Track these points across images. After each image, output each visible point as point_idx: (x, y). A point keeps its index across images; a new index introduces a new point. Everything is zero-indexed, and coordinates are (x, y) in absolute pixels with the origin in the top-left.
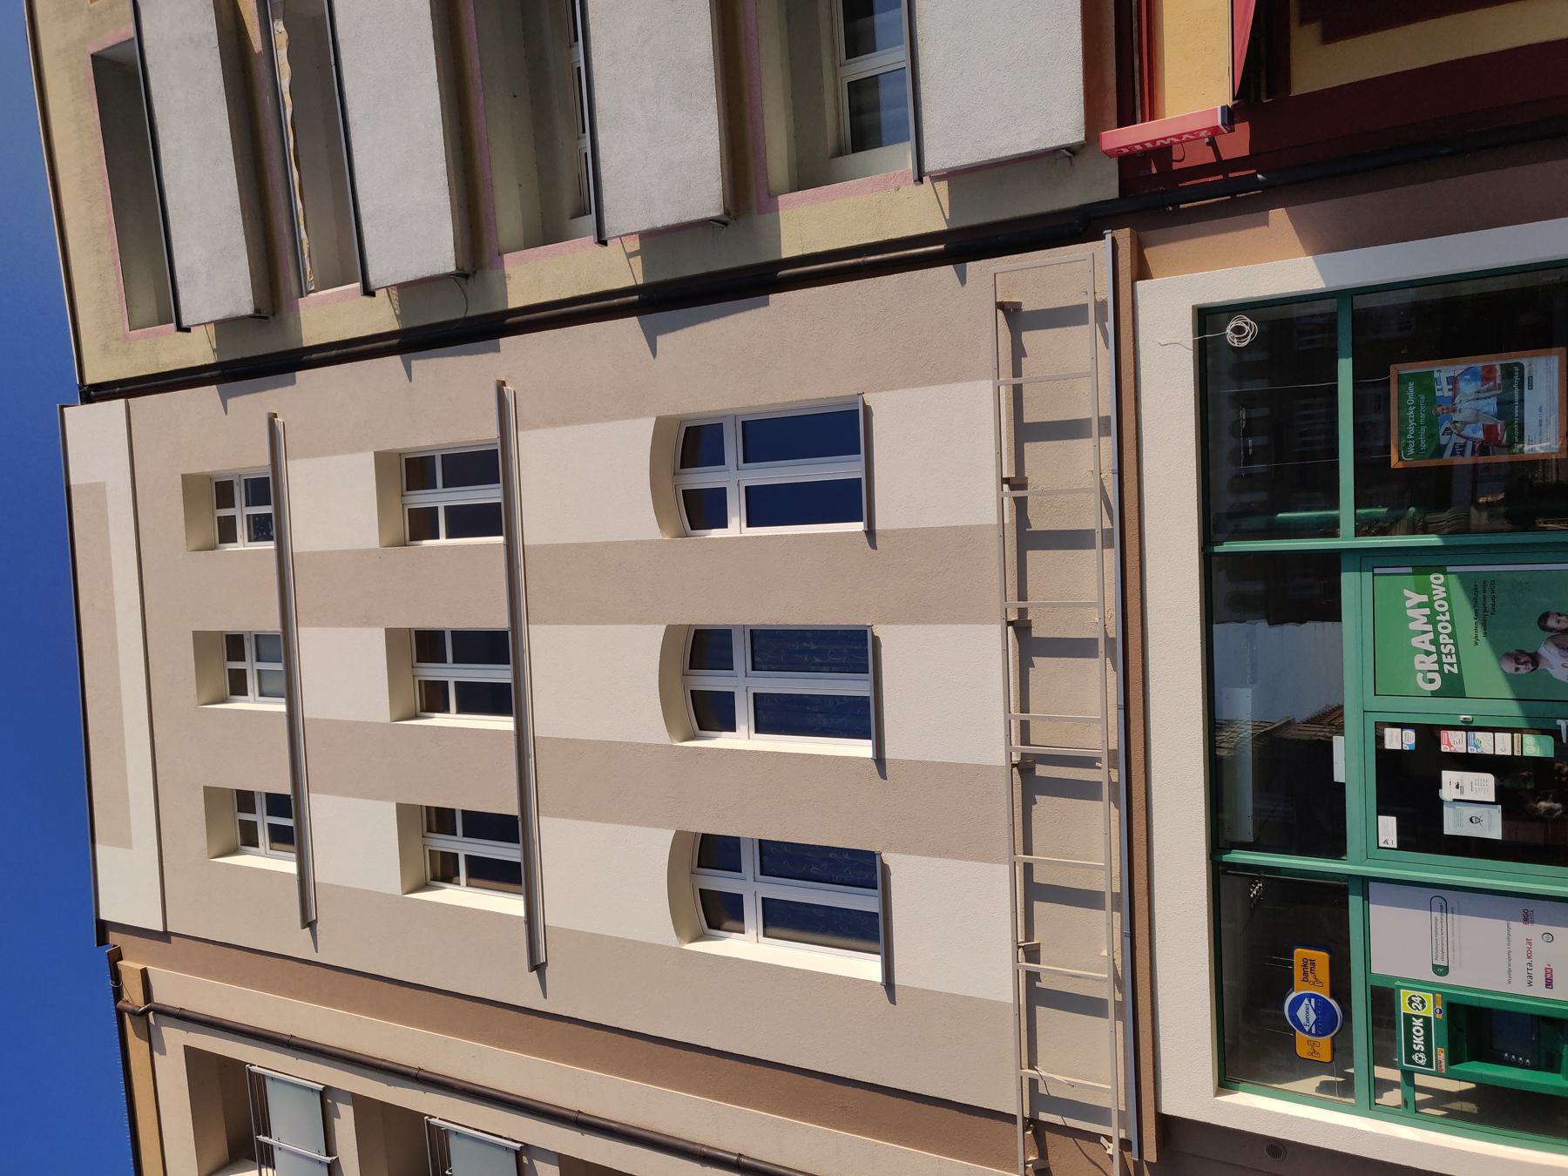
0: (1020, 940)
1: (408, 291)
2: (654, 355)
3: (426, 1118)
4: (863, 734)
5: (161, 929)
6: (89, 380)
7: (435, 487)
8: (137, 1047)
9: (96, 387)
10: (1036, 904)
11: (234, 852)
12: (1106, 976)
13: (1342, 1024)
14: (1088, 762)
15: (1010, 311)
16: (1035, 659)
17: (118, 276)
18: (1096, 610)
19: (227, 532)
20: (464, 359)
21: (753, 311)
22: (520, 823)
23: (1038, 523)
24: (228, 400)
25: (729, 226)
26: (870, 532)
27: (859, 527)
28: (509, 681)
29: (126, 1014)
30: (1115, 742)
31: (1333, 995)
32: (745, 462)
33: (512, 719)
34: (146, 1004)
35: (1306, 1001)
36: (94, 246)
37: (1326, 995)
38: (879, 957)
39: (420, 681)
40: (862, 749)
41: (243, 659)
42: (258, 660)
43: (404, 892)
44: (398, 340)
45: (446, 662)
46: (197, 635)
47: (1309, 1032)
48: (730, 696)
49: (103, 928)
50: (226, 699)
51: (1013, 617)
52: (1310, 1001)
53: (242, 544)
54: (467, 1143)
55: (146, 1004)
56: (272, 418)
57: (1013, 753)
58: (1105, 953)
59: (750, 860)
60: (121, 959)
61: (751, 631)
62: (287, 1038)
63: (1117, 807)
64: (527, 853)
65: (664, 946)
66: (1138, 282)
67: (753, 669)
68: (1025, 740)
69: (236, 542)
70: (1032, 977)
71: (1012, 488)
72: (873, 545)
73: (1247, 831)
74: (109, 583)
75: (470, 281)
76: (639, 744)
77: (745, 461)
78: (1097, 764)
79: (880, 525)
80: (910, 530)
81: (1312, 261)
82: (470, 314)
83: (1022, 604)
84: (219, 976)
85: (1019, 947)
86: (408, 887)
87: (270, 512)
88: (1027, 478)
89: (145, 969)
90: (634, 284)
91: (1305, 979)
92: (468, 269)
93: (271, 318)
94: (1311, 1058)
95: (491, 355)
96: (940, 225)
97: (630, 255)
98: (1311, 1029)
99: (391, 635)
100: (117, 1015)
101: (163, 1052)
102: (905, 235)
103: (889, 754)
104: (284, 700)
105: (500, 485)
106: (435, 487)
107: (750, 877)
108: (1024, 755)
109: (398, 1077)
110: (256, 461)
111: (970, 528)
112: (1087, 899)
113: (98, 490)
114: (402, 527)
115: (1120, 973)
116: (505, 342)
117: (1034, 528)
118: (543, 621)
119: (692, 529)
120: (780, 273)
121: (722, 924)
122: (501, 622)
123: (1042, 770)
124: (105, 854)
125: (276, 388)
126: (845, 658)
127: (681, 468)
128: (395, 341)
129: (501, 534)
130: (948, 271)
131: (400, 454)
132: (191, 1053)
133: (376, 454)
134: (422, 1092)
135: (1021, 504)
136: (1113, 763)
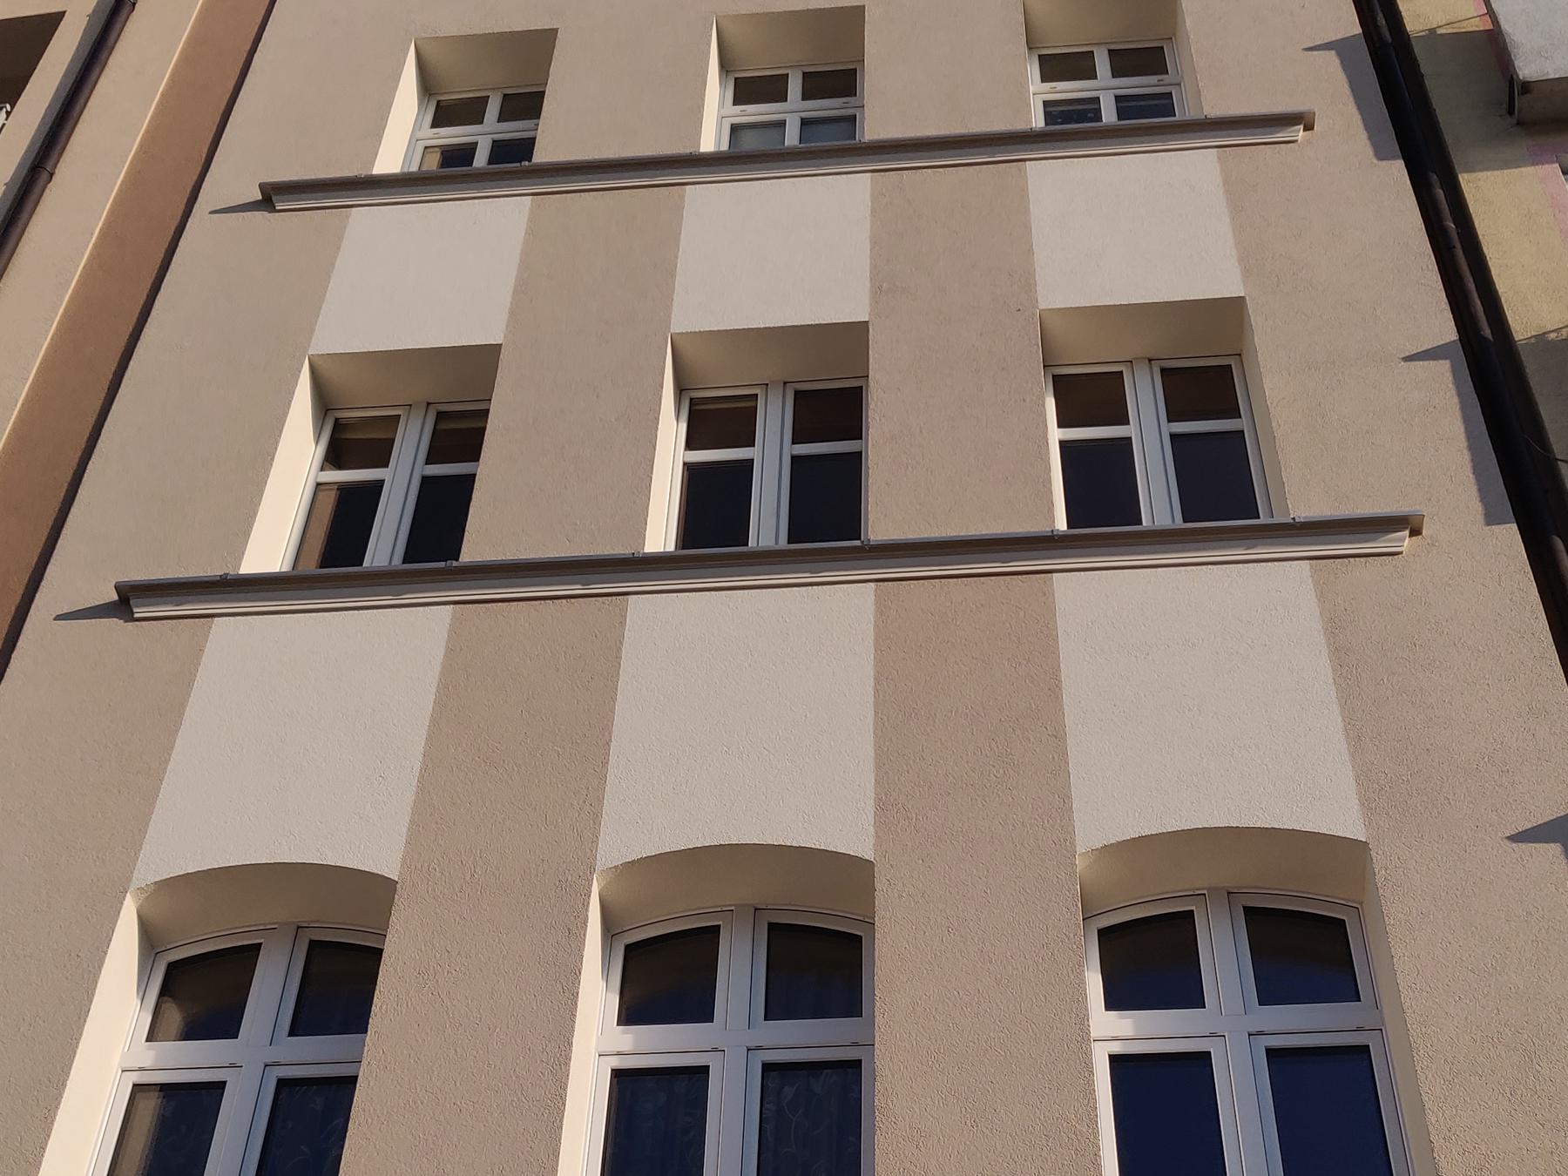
22: (442, 564)
24: (1333, 52)
28: (752, 542)
33: (671, 547)
42: (805, 123)
44: (1490, 337)
48: (703, 1013)
56: (1303, 120)
61: (857, 1064)
64: (384, 580)
69: (1042, 81)
77: (1271, 1053)
87: (1144, 524)
93: (1513, 120)
95: (1477, 507)
104: (724, 147)
105: (1179, 523)
107: (272, 1055)
114: (1085, 359)
122: (880, 525)
128: (1487, 332)
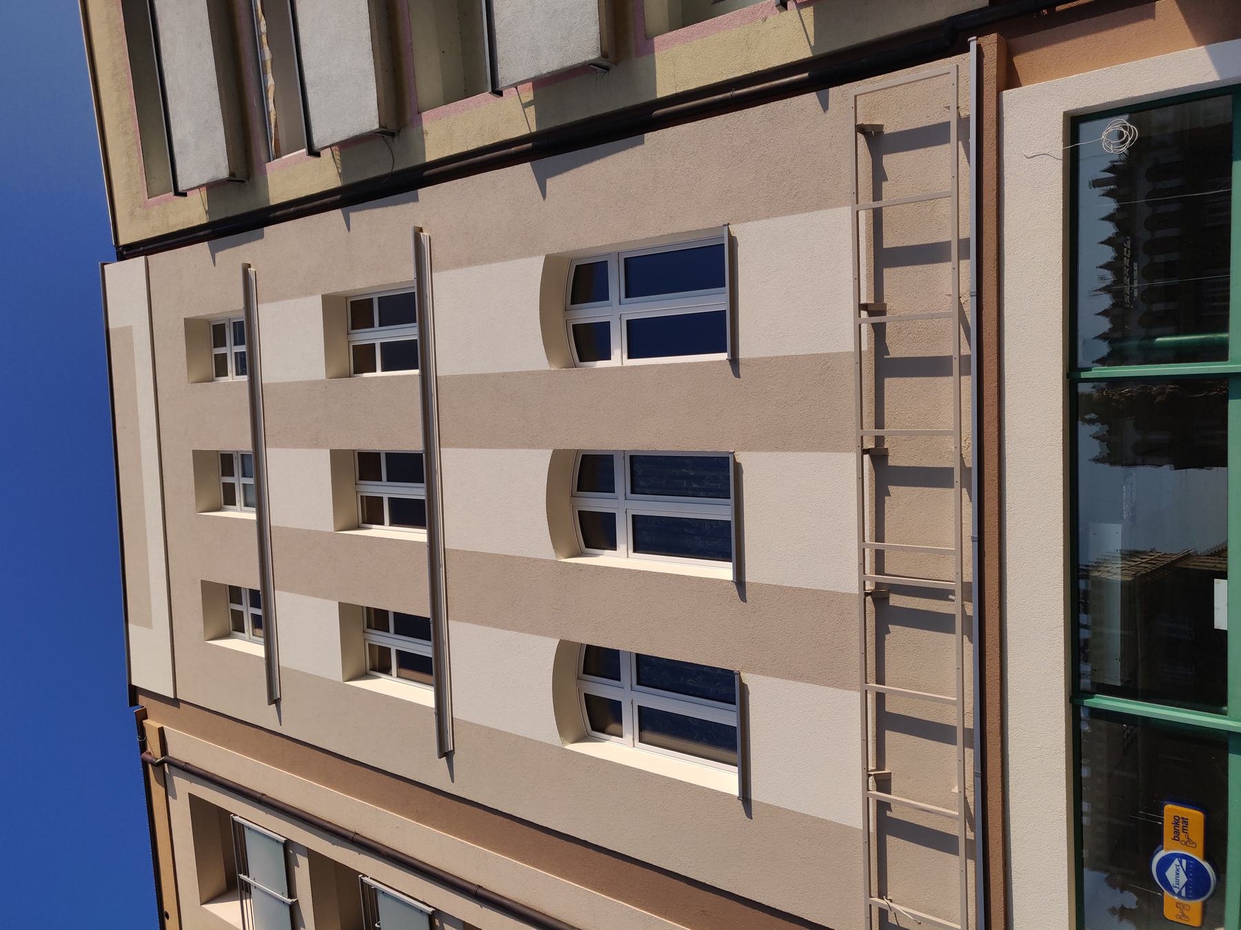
0: (871, 768)
1: (349, 147)
2: (544, 196)
3: (360, 876)
4: (723, 555)
6: (122, 242)
7: (373, 326)
8: (157, 790)
9: (129, 247)
10: (887, 381)
11: (226, 635)
12: (957, 813)
13: (1215, 890)
14: (942, 594)
15: (873, 136)
16: (891, 488)
17: (139, 153)
18: (952, 440)
19: (221, 370)
21: (630, 151)
22: (431, 625)
23: (897, 350)
25: (610, 71)
26: (734, 361)
27: (724, 356)
29: (150, 765)
30: (970, 575)
31: (1207, 857)
32: (627, 296)
34: (162, 756)
35: (1176, 862)
36: (122, 128)
37: (1199, 857)
38: (737, 768)
39: (361, 496)
40: (723, 571)
42: (244, 475)
43: (346, 678)
45: (381, 481)
46: (195, 453)
47: (1179, 895)
49: (134, 692)
51: (870, 445)
52: (1181, 862)
53: (231, 378)
54: (389, 901)
55: (162, 756)
57: (866, 582)
58: (956, 790)
59: (628, 671)
60: (146, 718)
63: (971, 641)
65: (549, 745)
66: (1004, 92)
67: (633, 492)
68: (879, 569)
70: (883, 806)
71: (871, 314)
72: (737, 373)
73: (1115, 677)
74: (135, 410)
75: (396, 139)
78: (951, 597)
79: (743, 354)
80: (772, 358)
81: (1204, 50)
82: (396, 169)
83: (879, 432)
85: (869, 775)
86: (352, 671)
87: (244, 350)
88: (886, 304)
89: (162, 727)
90: (529, 132)
91: (1176, 838)
92: (391, 127)
94: (1179, 921)
96: (803, 52)
97: (525, 106)
98: (1180, 892)
99: (336, 456)
101: (175, 797)
102: (770, 66)
103: (749, 578)
104: (254, 509)
105: (416, 324)
106: (373, 326)
108: (878, 585)
109: (339, 839)
110: (233, 305)
111: (828, 355)
112: (939, 732)
113: (128, 331)
114: (348, 361)
115: (972, 811)
116: (423, 192)
117: (892, 356)
119: (581, 361)
120: (655, 112)
121: (606, 727)
123: (896, 600)
124: (136, 632)
126: (720, 484)
127: (572, 304)
128: (338, 197)
129: (417, 368)
130: (811, 99)
131: (346, 298)
132: (194, 800)
135: (879, 331)
136: (966, 597)
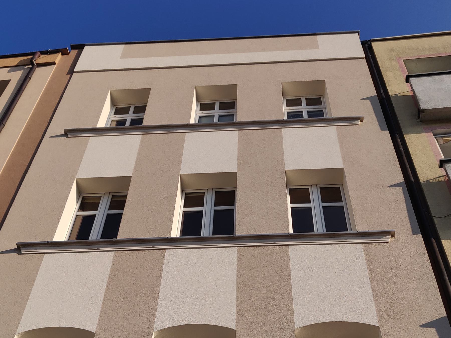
5: (75, 70)
8: (15, 61)
9: (371, 48)
17: (432, 55)
20: (406, 215)
22: (112, 239)
33: (178, 236)
34: (36, 64)
41: (220, 109)
44: (413, 181)
45: (215, 206)
49: (80, 48)
50: (199, 102)
55: (36, 64)
56: (361, 119)
62: (4, 123)
64: (95, 244)
65: (19, 324)
69: (287, 106)
76: (156, 311)
82: (435, 219)
84: (45, 94)
89: (55, 64)
99: (233, 176)
100: (33, 52)
101: (9, 71)
104: (197, 122)
105: (325, 232)
114: (298, 185)
118: (239, 255)
120: (433, 239)
125: (378, 121)
133: (342, 169)
134: (18, 80)
